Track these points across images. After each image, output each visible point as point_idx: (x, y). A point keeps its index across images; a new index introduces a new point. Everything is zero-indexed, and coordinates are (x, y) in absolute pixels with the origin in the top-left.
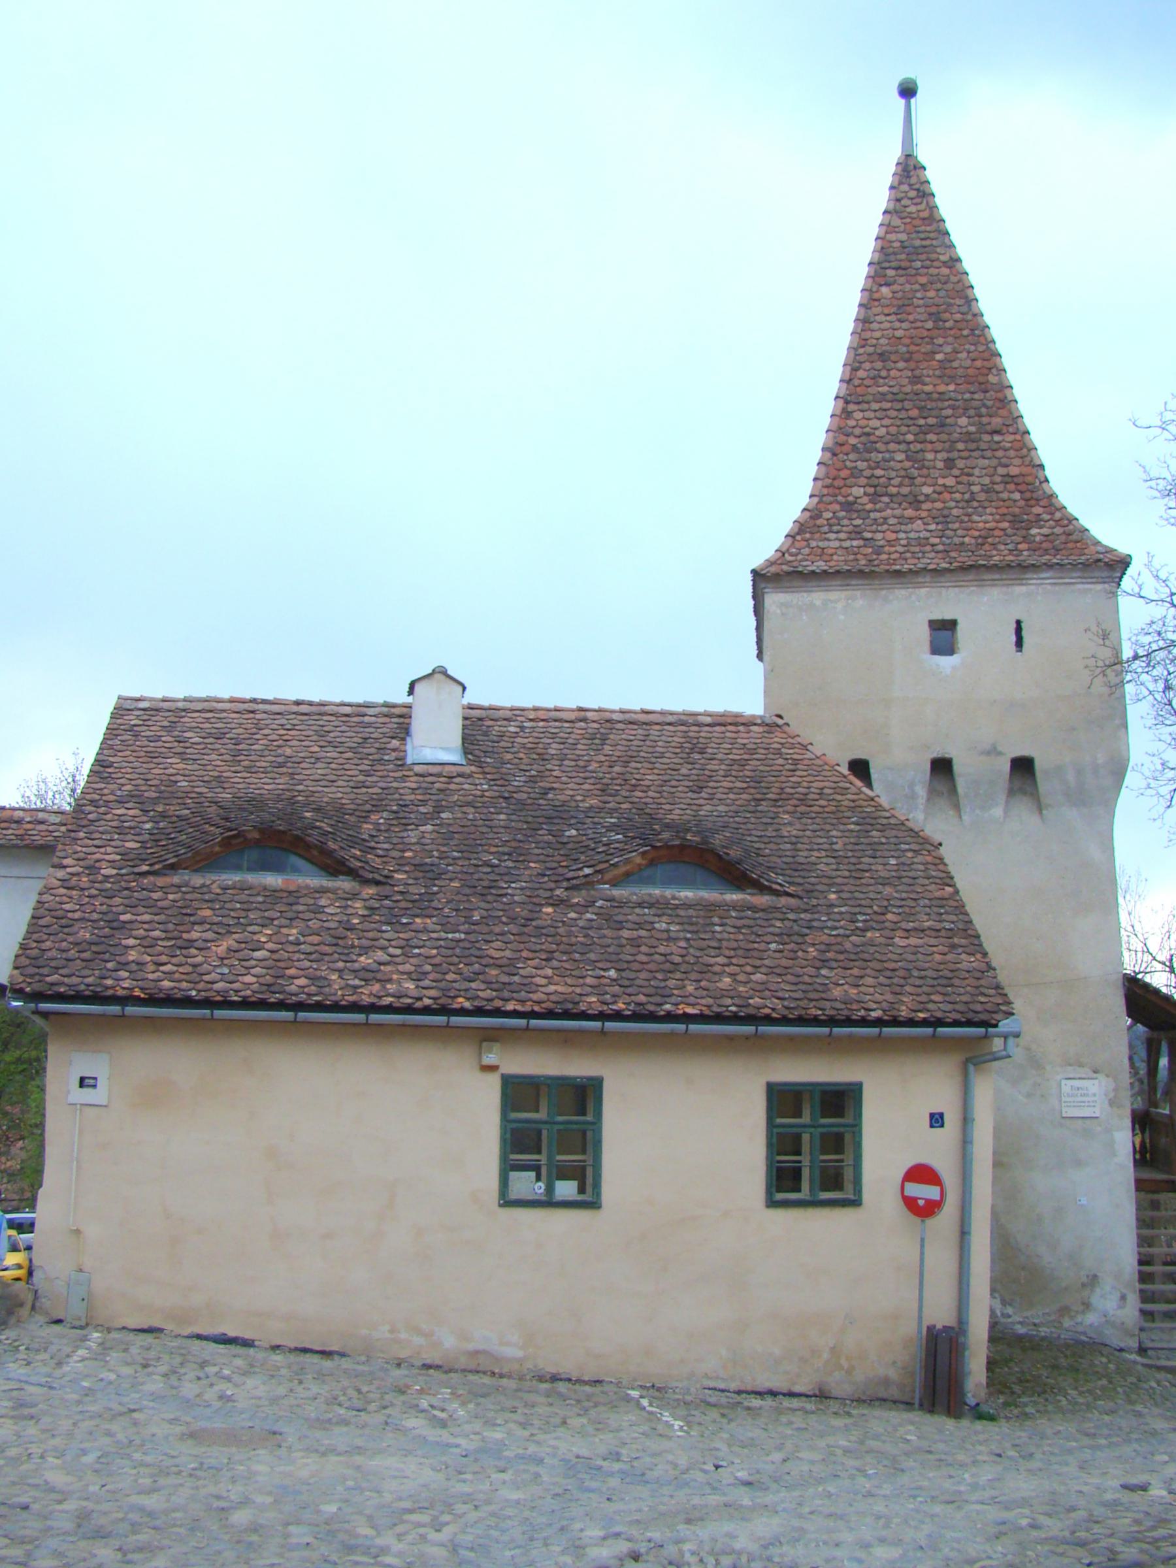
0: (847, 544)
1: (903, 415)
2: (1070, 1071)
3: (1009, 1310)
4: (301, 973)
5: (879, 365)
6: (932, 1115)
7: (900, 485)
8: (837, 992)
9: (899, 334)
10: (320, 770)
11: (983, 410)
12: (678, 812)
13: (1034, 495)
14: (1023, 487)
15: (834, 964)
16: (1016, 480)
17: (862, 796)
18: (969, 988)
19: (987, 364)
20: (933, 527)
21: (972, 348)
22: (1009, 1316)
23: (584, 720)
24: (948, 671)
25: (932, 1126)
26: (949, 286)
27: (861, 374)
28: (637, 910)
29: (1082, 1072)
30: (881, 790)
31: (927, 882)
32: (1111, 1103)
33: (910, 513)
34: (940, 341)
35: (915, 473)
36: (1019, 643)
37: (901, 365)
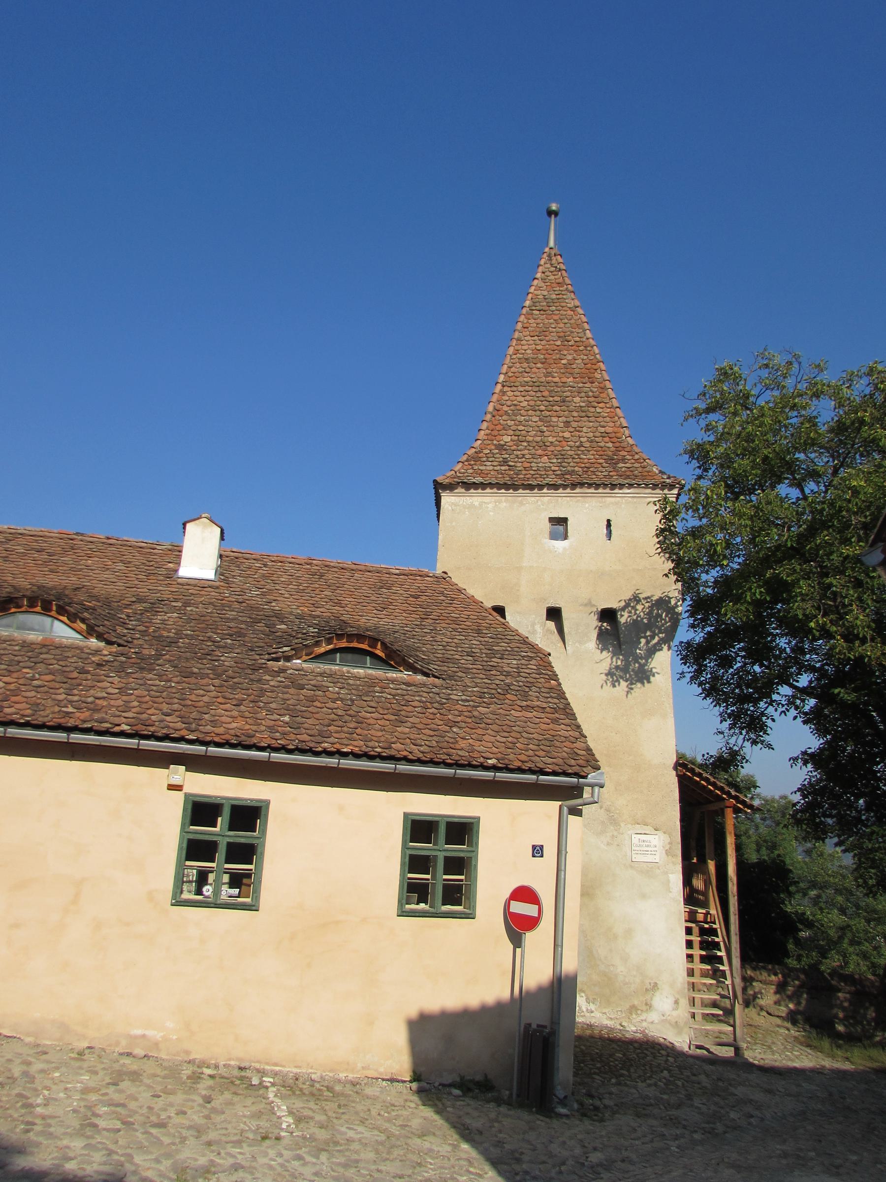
0: (498, 468)
1: (539, 394)
2: (639, 828)
3: (592, 1007)
4: (25, 700)
5: (525, 365)
6: (534, 847)
7: (536, 435)
8: (462, 744)
9: (539, 347)
10: (106, 575)
11: (591, 394)
12: (364, 620)
13: (622, 445)
14: (615, 440)
15: (463, 725)
16: (610, 435)
17: (497, 622)
18: (565, 749)
19: (595, 367)
20: (555, 461)
21: (585, 357)
22: (592, 1012)
23: (310, 564)
24: (561, 550)
25: (534, 856)
26: (572, 321)
27: (513, 369)
28: (319, 678)
29: (648, 829)
30: (512, 619)
31: (538, 676)
32: (668, 853)
33: (540, 452)
34: (565, 352)
35: (545, 429)
36: (609, 535)
37: (539, 365)
